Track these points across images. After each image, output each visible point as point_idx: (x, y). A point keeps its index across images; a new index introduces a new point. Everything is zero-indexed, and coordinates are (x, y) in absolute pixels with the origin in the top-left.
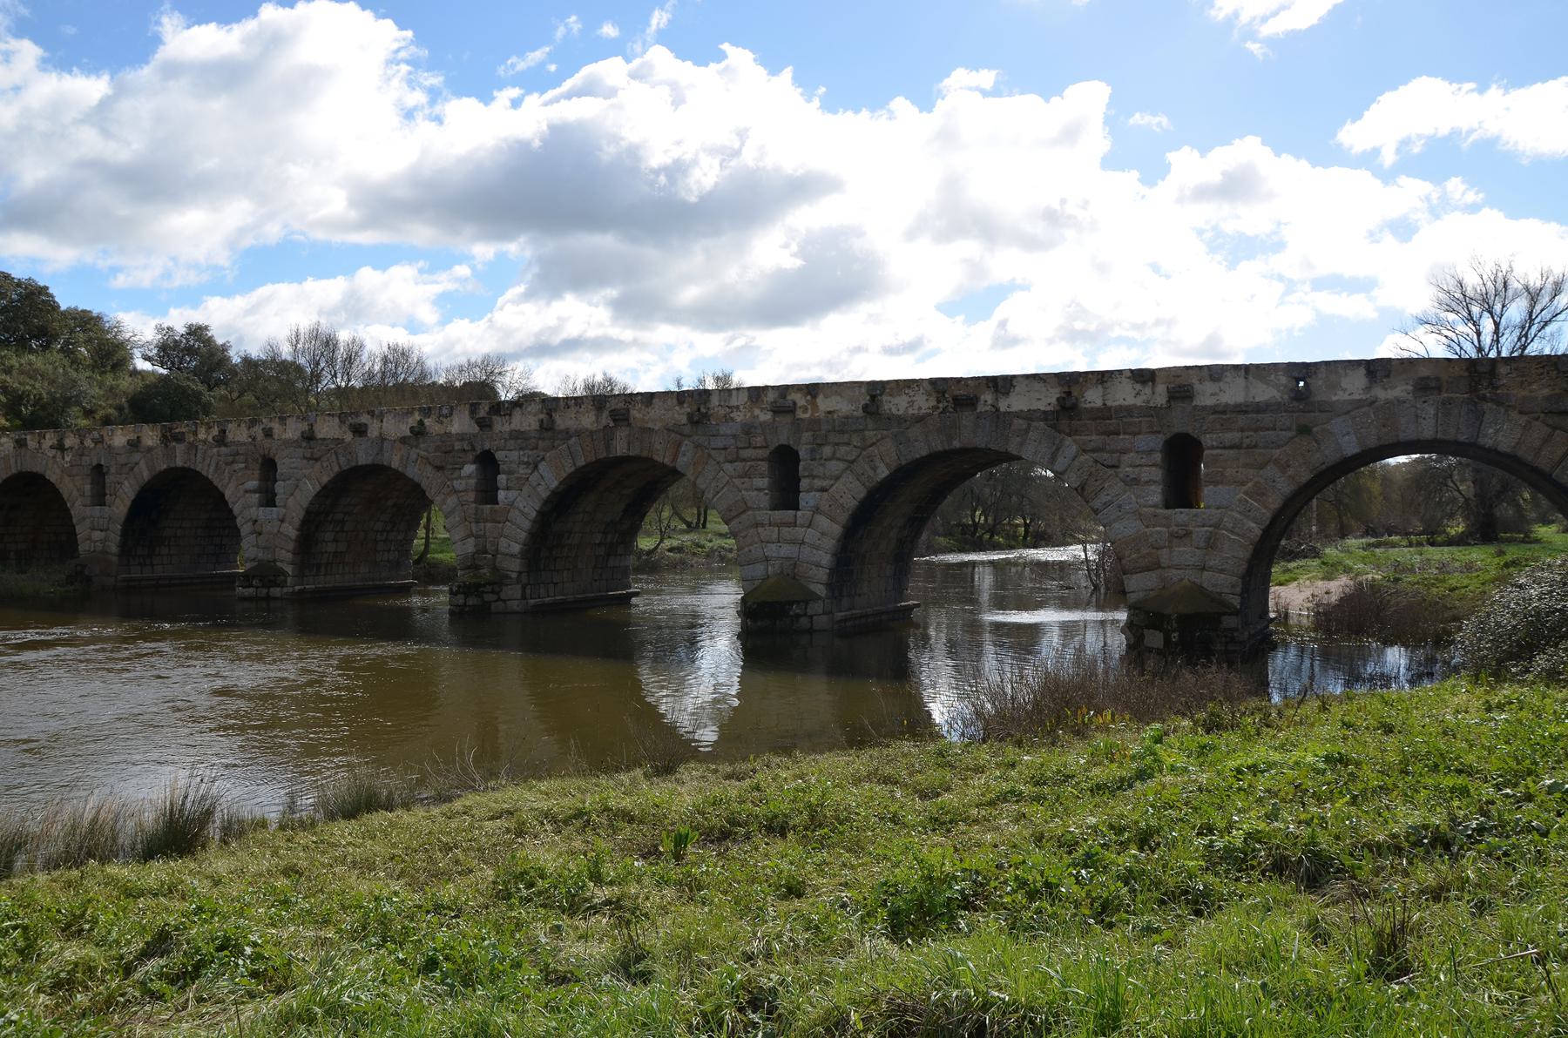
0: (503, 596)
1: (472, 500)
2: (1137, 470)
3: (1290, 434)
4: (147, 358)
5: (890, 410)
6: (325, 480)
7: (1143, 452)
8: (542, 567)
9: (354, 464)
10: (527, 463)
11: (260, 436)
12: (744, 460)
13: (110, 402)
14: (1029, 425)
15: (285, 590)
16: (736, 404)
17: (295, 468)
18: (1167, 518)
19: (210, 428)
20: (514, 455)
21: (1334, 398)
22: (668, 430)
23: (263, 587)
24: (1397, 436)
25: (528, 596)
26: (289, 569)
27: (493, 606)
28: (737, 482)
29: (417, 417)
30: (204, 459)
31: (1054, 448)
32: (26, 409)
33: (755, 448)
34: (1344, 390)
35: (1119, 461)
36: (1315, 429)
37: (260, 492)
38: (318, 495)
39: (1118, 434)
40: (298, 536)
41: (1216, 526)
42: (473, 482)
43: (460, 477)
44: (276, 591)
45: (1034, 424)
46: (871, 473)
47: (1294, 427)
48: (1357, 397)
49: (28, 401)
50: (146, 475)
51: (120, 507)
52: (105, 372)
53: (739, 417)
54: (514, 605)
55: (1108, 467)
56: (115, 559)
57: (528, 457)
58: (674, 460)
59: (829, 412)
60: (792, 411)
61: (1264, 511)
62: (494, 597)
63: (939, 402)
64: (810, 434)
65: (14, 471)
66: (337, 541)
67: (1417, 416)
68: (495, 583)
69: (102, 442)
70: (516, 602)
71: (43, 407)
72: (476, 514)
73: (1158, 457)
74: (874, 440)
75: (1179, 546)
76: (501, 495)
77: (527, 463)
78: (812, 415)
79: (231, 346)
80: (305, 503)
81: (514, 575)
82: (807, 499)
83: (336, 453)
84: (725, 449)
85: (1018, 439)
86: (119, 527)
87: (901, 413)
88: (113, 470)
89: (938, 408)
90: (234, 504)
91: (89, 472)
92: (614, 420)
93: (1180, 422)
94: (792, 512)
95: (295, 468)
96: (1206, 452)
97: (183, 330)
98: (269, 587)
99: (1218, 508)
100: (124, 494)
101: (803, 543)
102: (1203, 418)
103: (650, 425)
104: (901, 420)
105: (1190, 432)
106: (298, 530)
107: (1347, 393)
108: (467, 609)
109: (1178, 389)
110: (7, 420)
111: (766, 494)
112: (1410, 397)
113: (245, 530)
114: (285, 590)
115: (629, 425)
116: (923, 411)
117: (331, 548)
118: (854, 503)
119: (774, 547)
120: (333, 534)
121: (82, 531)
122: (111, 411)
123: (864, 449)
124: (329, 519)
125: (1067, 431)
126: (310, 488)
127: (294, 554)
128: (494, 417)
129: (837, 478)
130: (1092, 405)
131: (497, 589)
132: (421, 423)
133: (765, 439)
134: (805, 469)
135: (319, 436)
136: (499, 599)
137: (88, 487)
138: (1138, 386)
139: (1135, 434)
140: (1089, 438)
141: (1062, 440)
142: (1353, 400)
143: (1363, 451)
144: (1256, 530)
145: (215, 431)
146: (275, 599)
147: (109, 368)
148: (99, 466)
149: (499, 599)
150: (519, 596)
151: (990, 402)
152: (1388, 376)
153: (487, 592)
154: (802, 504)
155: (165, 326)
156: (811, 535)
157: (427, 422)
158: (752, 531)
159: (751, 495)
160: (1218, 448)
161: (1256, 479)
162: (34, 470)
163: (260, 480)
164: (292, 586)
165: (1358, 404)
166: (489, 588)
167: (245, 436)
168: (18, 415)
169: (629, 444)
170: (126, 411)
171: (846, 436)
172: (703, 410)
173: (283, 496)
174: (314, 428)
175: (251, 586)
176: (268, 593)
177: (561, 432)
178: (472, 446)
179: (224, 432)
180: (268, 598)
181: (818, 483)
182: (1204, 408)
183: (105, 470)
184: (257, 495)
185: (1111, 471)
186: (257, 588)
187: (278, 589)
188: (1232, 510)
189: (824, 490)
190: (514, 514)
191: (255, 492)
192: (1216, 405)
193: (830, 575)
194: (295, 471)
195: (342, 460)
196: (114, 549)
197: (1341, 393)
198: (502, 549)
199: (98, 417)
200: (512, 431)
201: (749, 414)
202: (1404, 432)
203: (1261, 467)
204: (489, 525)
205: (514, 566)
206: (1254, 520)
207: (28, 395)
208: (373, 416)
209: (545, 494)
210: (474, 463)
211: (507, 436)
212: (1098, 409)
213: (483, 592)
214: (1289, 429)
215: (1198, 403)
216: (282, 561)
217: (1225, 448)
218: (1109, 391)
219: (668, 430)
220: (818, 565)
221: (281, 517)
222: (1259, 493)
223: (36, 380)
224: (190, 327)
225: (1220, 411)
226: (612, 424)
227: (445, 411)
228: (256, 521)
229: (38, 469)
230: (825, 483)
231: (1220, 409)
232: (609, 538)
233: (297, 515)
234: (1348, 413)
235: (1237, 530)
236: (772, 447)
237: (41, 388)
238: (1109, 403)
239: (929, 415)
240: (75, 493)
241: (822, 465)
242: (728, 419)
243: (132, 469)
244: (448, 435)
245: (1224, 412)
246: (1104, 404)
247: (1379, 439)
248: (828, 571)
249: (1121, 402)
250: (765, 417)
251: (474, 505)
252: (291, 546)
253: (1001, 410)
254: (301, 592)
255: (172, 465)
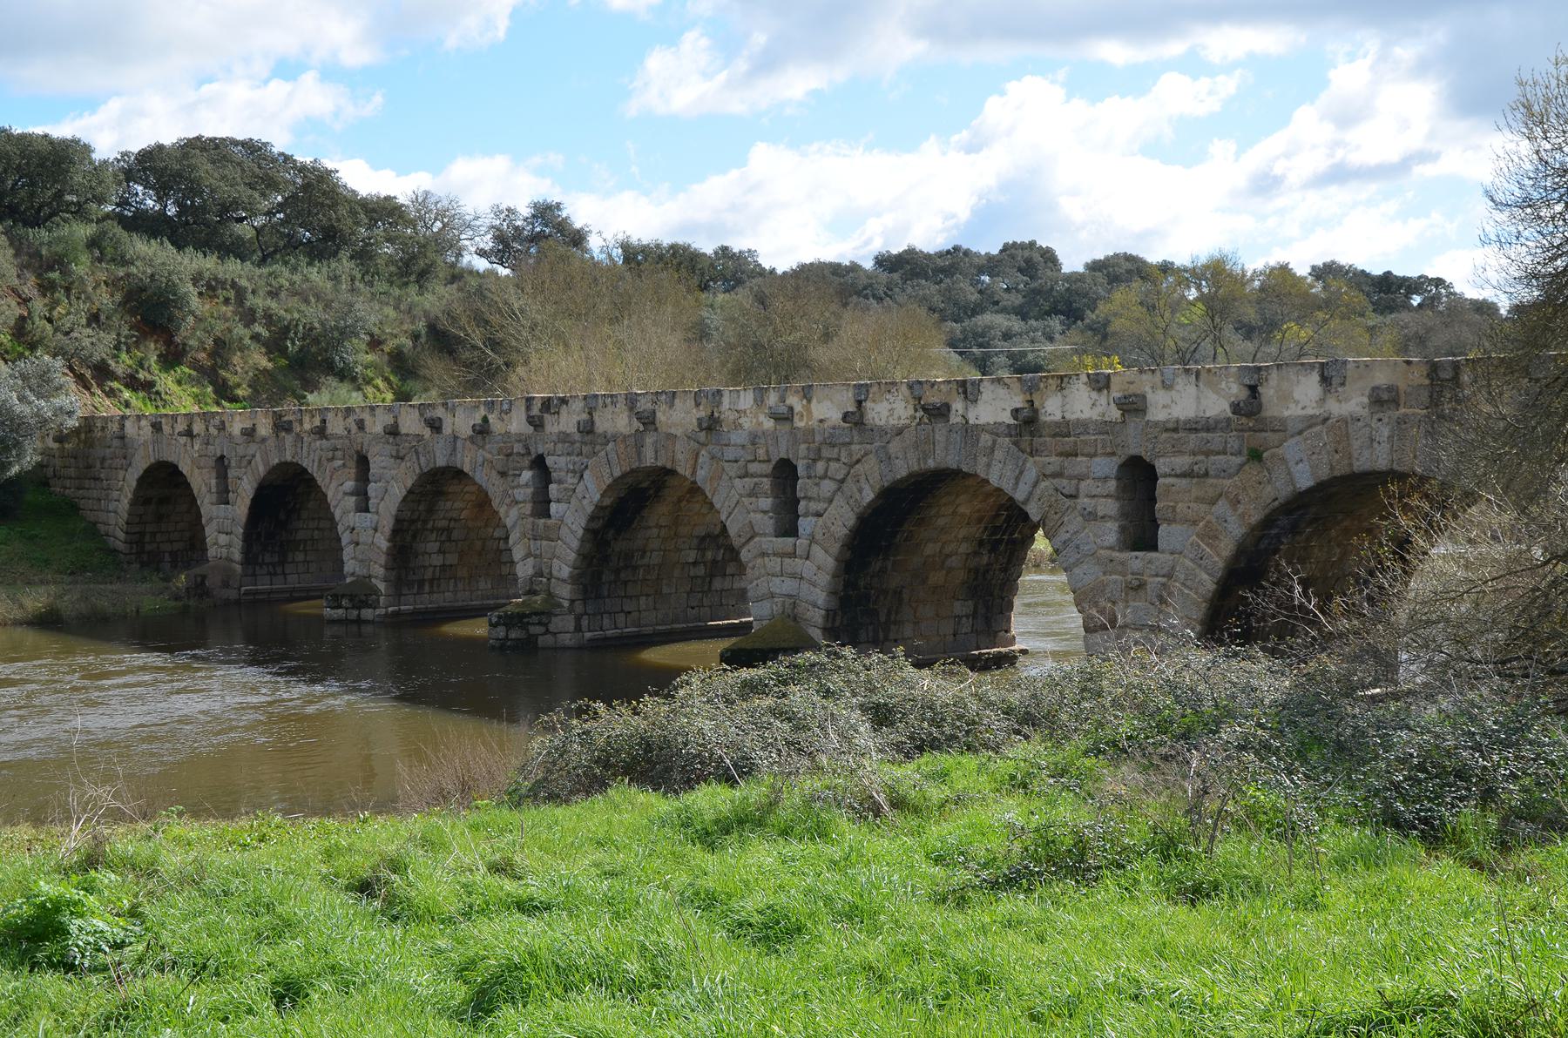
0: (552, 628)
1: (528, 512)
2: (1093, 501)
3: (1238, 460)
4: (482, 253)
5: (873, 419)
6: (409, 483)
7: (1099, 479)
8: (606, 593)
9: (432, 466)
10: (574, 472)
11: (354, 428)
12: (752, 476)
13: (405, 327)
14: (994, 442)
15: (378, 612)
16: (743, 408)
17: (385, 468)
18: (1122, 563)
19: (313, 416)
20: (562, 461)
21: (1286, 413)
22: (689, 438)
23: (353, 608)
24: (1351, 465)
25: (584, 628)
26: (382, 586)
27: (540, 639)
28: (746, 501)
29: (482, 411)
30: (309, 454)
31: (1017, 471)
32: (293, 343)
33: (760, 461)
34: (1297, 402)
35: (1078, 489)
36: (1265, 455)
37: (357, 495)
38: (405, 499)
39: (1076, 455)
40: (388, 548)
41: (1169, 576)
42: (530, 491)
43: (519, 486)
44: (367, 614)
45: (1000, 440)
46: (857, 496)
47: (1245, 451)
48: (1310, 412)
49: (296, 333)
50: (262, 470)
51: (241, 508)
52: (406, 284)
53: (747, 423)
54: (567, 639)
55: (1066, 496)
56: (238, 568)
57: (574, 463)
58: (694, 473)
59: (821, 421)
60: (787, 419)
61: (1217, 559)
62: (540, 629)
63: (916, 410)
64: (806, 445)
65: (152, 460)
66: (444, 553)
67: (1372, 440)
68: (543, 613)
69: (224, 429)
70: (568, 635)
71: (316, 341)
72: (533, 530)
73: (1112, 485)
74: (859, 456)
75: (1134, 600)
76: (553, 507)
77: (574, 472)
78: (807, 423)
79: (590, 232)
80: (394, 510)
81: (566, 604)
82: (805, 525)
83: (417, 453)
84: (736, 461)
85: (985, 459)
86: (242, 531)
87: (883, 423)
88: (233, 463)
89: (915, 418)
90: (336, 507)
91: (214, 464)
92: (644, 424)
93: (1135, 445)
94: (791, 540)
95: (385, 468)
96: (1160, 481)
97: (525, 211)
98: (359, 608)
99: (1172, 553)
100: (245, 489)
101: (802, 578)
102: (1156, 437)
103: (673, 431)
104: (883, 431)
105: (1143, 454)
106: (389, 541)
107: (1300, 406)
108: (509, 643)
109: (1123, 401)
110: (270, 360)
111: (771, 518)
112: (1365, 412)
113: (345, 538)
114: (378, 612)
115: (656, 430)
116: (902, 422)
117: (437, 560)
118: (846, 531)
119: (777, 580)
120: (438, 544)
121: (210, 532)
122: (403, 340)
123: (852, 466)
124: (430, 526)
125: (1028, 450)
126: (398, 492)
127: (386, 569)
128: (545, 415)
129: (831, 501)
130: (1052, 418)
131: (545, 620)
132: (485, 420)
133: (767, 451)
134: (801, 490)
135: (403, 431)
136: (547, 632)
137: (213, 482)
138: (1094, 395)
139: (1091, 456)
140: (1047, 459)
141: (1025, 461)
142: (1305, 417)
143: (1318, 484)
144: (1208, 583)
145: (317, 422)
146: (367, 622)
147: (413, 278)
148: (222, 457)
149: (547, 632)
150: (572, 628)
151: (960, 412)
152: (1343, 384)
153: (533, 624)
154: (801, 530)
155: (503, 207)
156: (807, 568)
157: (491, 419)
158: (759, 561)
159: (757, 518)
160: (1170, 475)
161: (1207, 518)
162: (170, 459)
163: (356, 480)
164: (385, 606)
165: (1311, 422)
166: (535, 619)
167: (342, 428)
168: (283, 351)
169: (656, 452)
170: (423, 340)
171: (836, 450)
172: (716, 414)
173: (375, 501)
174: (399, 420)
175: (340, 607)
176: (359, 615)
177: (600, 435)
178: (528, 449)
179: (325, 421)
180: (359, 621)
181: (814, 506)
182: (1156, 424)
183: (226, 463)
184: (354, 498)
185: (1068, 502)
186: (347, 609)
187: (370, 610)
188: (1185, 557)
189: (819, 515)
190: (564, 531)
191: (352, 494)
192: (1168, 421)
193: (827, 617)
194: (386, 471)
195: (422, 460)
196: (237, 556)
197: (1292, 406)
198: (555, 573)
199: (387, 349)
200: (560, 433)
201: (754, 421)
202: (1358, 460)
203: (1213, 502)
204: (544, 543)
205: (564, 592)
206: (1206, 569)
207: (297, 325)
208: (447, 409)
209: (590, 509)
210: (531, 468)
211: (554, 438)
212: (1057, 424)
213: (528, 623)
214: (1240, 453)
215: (1151, 418)
216: (376, 577)
217: (1177, 476)
218: (1067, 400)
219: (689, 438)
220: (815, 605)
221: (373, 526)
222: (1211, 536)
223: (307, 301)
224: (536, 206)
225: (1175, 427)
226: (642, 429)
227: (505, 407)
228: (353, 529)
229: (172, 459)
230: (820, 506)
231: (1170, 425)
232: (709, 555)
233: (387, 524)
234: (1300, 433)
235: (1189, 583)
236: (775, 460)
237: (313, 314)
238: (1068, 416)
239: (908, 427)
240: (203, 488)
241: (817, 484)
242: (737, 426)
243: (250, 462)
244: (508, 433)
245: (1175, 430)
246: (1063, 417)
247: (1332, 468)
248: (823, 612)
249: (1078, 415)
250: (769, 424)
251: (532, 519)
252: (382, 559)
253: (970, 422)
254: (396, 614)
255: (283, 460)
